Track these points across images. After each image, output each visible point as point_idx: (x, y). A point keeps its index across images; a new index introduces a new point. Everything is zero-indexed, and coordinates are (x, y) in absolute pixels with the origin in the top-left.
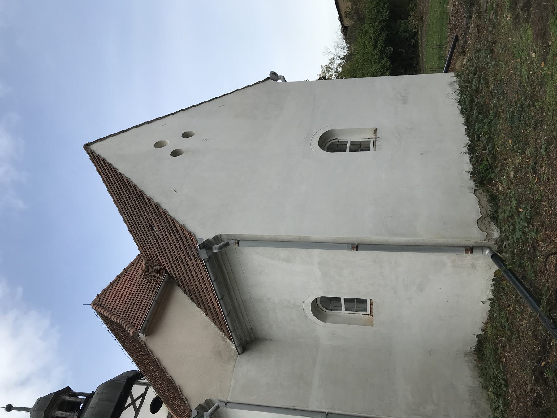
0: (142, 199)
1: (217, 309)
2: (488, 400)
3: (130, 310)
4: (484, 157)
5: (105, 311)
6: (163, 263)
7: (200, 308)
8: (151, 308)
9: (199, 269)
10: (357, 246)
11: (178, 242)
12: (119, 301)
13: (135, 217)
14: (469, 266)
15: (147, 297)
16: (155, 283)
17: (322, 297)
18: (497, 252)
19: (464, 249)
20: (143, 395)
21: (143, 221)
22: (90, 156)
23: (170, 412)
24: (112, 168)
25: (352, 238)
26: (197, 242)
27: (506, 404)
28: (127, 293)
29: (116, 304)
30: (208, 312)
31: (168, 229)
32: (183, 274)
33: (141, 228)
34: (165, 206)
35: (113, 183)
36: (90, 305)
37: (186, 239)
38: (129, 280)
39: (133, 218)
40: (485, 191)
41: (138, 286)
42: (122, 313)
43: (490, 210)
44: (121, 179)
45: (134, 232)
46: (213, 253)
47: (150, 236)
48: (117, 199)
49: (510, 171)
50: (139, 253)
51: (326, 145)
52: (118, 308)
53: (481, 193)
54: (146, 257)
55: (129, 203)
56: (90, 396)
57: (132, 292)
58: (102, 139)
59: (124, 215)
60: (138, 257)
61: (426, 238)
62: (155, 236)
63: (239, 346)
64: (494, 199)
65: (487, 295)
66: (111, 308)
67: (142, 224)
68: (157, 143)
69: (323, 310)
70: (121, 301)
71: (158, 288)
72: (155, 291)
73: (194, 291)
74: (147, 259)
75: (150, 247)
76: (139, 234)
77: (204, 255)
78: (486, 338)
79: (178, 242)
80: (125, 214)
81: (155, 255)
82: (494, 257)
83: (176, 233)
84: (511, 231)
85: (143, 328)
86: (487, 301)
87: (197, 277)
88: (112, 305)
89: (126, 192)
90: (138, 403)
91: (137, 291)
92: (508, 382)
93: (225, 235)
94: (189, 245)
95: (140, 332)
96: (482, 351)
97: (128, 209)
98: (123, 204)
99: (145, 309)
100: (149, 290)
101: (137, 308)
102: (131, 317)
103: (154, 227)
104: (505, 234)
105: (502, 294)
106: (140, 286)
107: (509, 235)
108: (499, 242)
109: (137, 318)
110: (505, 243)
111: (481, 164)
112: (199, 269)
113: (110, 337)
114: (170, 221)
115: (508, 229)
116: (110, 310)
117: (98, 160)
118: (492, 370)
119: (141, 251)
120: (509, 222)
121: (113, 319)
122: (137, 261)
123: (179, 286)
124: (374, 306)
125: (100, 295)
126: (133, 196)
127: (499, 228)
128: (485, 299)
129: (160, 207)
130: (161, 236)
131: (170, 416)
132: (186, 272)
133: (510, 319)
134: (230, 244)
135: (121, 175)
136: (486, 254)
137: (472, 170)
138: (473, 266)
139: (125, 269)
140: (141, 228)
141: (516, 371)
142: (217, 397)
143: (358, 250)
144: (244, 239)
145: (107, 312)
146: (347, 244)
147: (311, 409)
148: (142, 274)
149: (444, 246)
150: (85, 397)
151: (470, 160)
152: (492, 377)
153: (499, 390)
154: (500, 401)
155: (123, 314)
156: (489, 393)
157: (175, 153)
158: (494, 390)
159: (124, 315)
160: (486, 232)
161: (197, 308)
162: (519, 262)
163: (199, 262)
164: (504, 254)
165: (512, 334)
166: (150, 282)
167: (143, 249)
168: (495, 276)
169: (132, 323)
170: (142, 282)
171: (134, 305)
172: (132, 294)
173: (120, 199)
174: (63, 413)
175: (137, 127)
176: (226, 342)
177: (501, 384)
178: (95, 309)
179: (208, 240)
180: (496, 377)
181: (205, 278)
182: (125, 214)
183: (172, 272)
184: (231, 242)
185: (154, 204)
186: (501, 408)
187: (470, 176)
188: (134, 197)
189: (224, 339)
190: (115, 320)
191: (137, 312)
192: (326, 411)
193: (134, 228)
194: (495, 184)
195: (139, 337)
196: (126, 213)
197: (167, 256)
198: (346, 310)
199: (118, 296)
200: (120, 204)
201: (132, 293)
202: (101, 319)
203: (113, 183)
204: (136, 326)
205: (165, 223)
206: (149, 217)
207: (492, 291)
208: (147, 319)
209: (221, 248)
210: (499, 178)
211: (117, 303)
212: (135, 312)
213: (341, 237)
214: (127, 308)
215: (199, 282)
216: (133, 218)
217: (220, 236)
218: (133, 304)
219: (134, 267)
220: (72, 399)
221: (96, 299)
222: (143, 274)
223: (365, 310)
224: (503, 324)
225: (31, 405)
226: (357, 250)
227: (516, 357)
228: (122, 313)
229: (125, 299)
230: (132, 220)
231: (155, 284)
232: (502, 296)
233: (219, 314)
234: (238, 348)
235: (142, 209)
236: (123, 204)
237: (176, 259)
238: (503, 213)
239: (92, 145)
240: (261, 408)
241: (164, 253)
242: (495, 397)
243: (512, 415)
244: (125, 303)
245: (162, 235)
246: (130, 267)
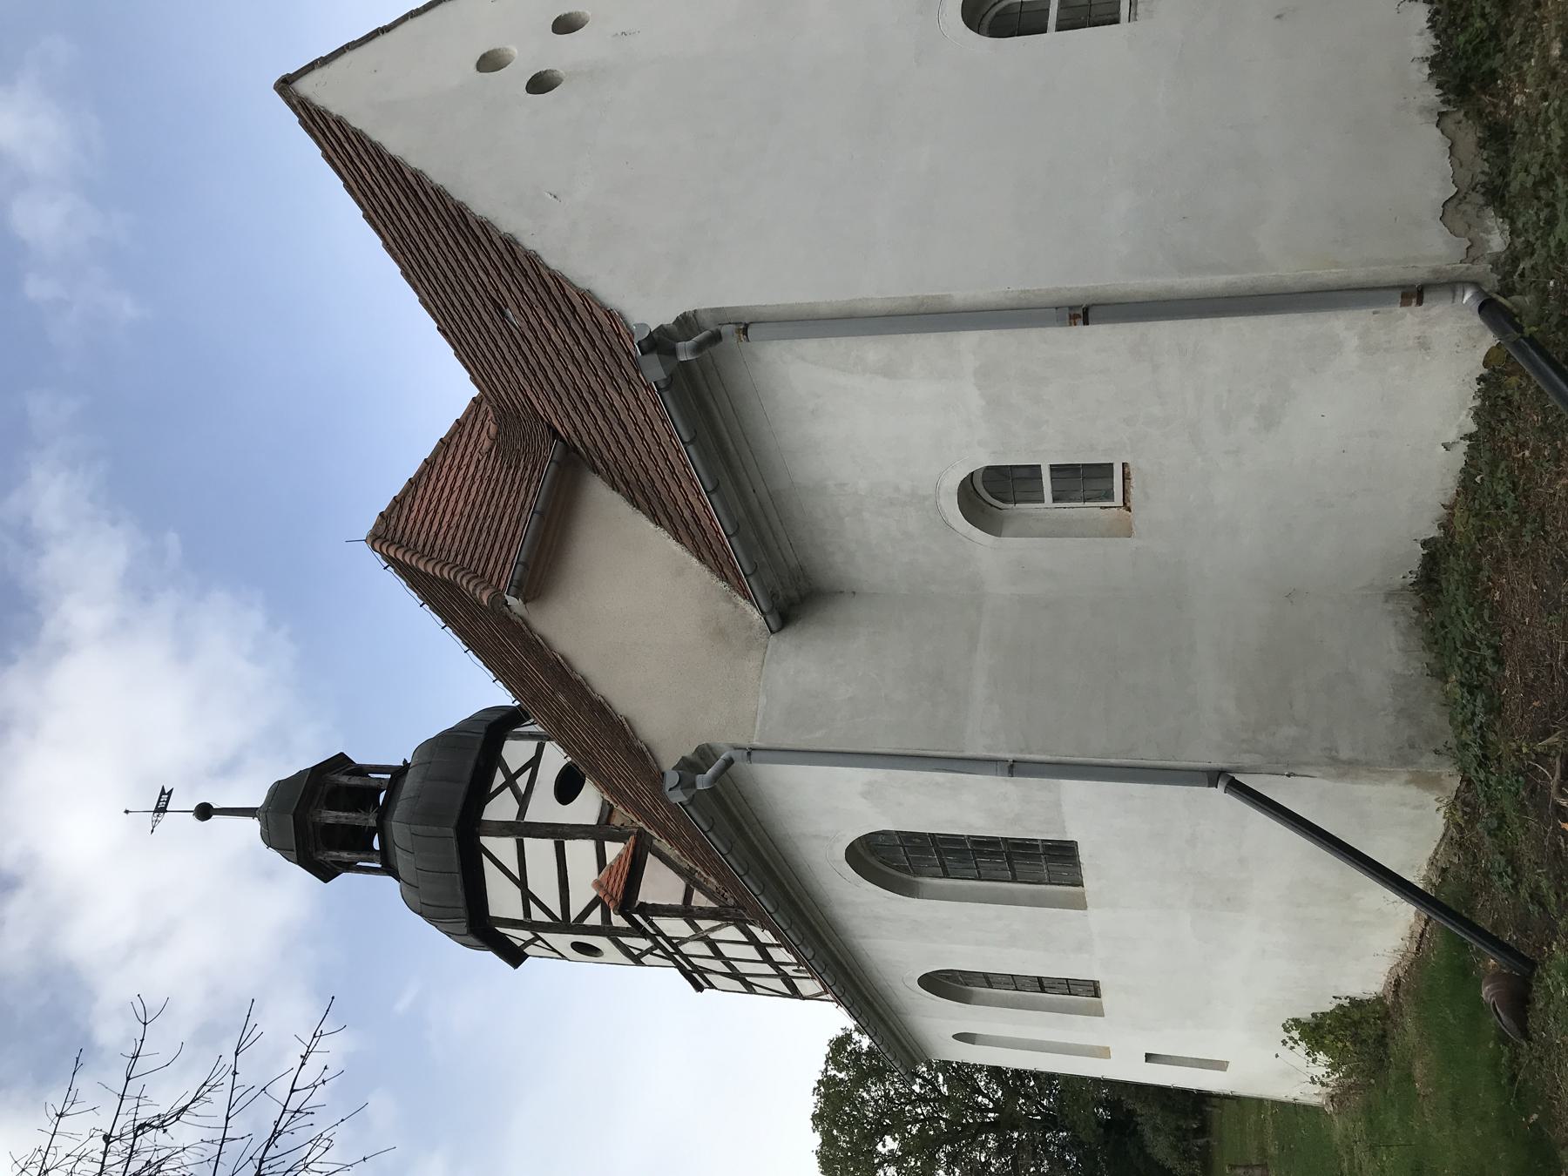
0: (463, 228)
1: (705, 522)
2: (1445, 705)
3: (472, 545)
4: (1472, 7)
5: (405, 552)
6: (545, 410)
7: (659, 523)
8: (549, 471)
9: (645, 414)
10: (1086, 311)
11: (579, 344)
12: (440, 524)
13: (452, 287)
14: (1410, 343)
15: (514, 506)
16: (529, 467)
17: (988, 468)
18: (1498, 293)
19: (1398, 294)
20: (534, 763)
21: (473, 295)
22: (299, 115)
23: (606, 797)
24: (368, 144)
25: (1069, 290)
26: (631, 335)
27: (1495, 709)
28: (457, 502)
29: (432, 533)
30: (682, 532)
31: (546, 309)
32: (603, 437)
33: (471, 318)
34: (530, 241)
35: (377, 190)
36: (365, 541)
37: (602, 332)
38: (459, 468)
39: (445, 291)
40: (1471, 114)
41: (485, 482)
42: (453, 554)
43: (1483, 172)
44: (397, 175)
45: (452, 332)
46: (678, 365)
47: (498, 338)
48: (394, 240)
49: (1551, 40)
50: (475, 392)
51: (984, 16)
52: (439, 541)
53: (1460, 122)
54: (497, 400)
55: (428, 248)
56: (399, 773)
57: (472, 497)
58: (324, 61)
59: (419, 286)
60: (473, 404)
61: (1285, 271)
62: (511, 334)
63: (771, 612)
64: (1497, 137)
65: (1460, 426)
66: (421, 543)
67: (472, 304)
68: (483, 57)
69: (992, 505)
70: (445, 524)
71: (539, 481)
72: (532, 489)
73: (638, 480)
74: (498, 405)
75: (501, 369)
76: (467, 335)
77: (654, 370)
78: (1449, 545)
79: (579, 344)
80: (420, 281)
81: (519, 392)
82: (1488, 309)
83: (570, 317)
84: (1541, 224)
85: (514, 583)
86: (1458, 442)
87: (643, 439)
88: (423, 536)
89: (418, 214)
90: (522, 782)
91: (485, 493)
92: (1503, 653)
93: (705, 310)
94: (611, 349)
95: (507, 594)
96: (1436, 582)
97: (427, 263)
98: (411, 252)
99: (514, 535)
100: (515, 488)
101: (491, 538)
102: (479, 560)
103: (508, 310)
104: (1523, 238)
105: (1503, 416)
106: (489, 481)
107: (1537, 239)
108: (1504, 264)
109: (496, 562)
110: (1521, 266)
111: (1464, 29)
112: (645, 414)
113: (429, 621)
114: (551, 283)
115: (1535, 218)
116: (420, 549)
117: (322, 126)
118: (1460, 626)
119: (478, 386)
120: (1538, 198)
121: (430, 570)
122: (472, 416)
123: (596, 470)
124: (1134, 482)
125: (385, 514)
126: (438, 221)
127: (1507, 220)
128: (1452, 435)
129: (518, 244)
130: (529, 334)
131: (608, 807)
132: (611, 429)
133: (1521, 482)
134: (723, 335)
135: (395, 161)
136: (1464, 302)
137: (1434, 53)
138: (1424, 345)
139: (441, 440)
140: (471, 318)
141: (1527, 619)
142: (725, 738)
143: (1090, 322)
144: (762, 319)
145: (413, 555)
146: (1057, 308)
147: (969, 753)
148: (491, 450)
149: (1341, 290)
150: (389, 776)
151: (1429, 20)
152: (1459, 645)
153: (1478, 676)
154: (1479, 703)
155: (456, 556)
156: (1448, 687)
157: (540, 84)
158: (1462, 675)
159: (460, 557)
160: (1467, 239)
161: (652, 526)
162: (1560, 315)
163: (642, 394)
164: (1515, 298)
165: (1523, 522)
166: (517, 467)
167: (483, 380)
168: (1485, 364)
169: (483, 574)
170: (493, 470)
171: (480, 530)
172: (473, 504)
173: (402, 238)
174: (341, 814)
175: (417, 15)
176: (736, 605)
177: (1484, 658)
178: (378, 550)
179: (661, 329)
180: (1470, 643)
181: (665, 438)
182: (420, 281)
183: (572, 433)
184: (725, 330)
185: (500, 237)
186: (1481, 718)
187: (1427, 71)
188: (440, 225)
189: (729, 599)
190: (438, 574)
191: (493, 546)
192: (1010, 756)
193: (453, 319)
194: (1504, 88)
195: (508, 606)
196: (422, 277)
197: (554, 390)
198: (1055, 500)
199: (436, 512)
200: (403, 254)
201: (470, 500)
202: (400, 575)
203: (377, 190)
204: (494, 582)
205: (536, 292)
206: (490, 281)
207: (1476, 413)
208: (521, 559)
209: (699, 348)
210: (1516, 70)
211: (434, 528)
212: (488, 546)
213: (1039, 290)
214: (465, 540)
215: (650, 452)
216: (445, 291)
217: (694, 316)
218: (477, 528)
219: (466, 432)
220: (356, 781)
221: (376, 526)
222: (494, 450)
223: (1109, 495)
224: (1501, 498)
225: (258, 801)
226: (1086, 323)
227: (1531, 580)
228: (453, 554)
229: (456, 518)
230: (443, 296)
231: (529, 469)
232: (1502, 422)
233: (710, 534)
234: (768, 618)
235: (467, 260)
236: (411, 252)
237: (579, 395)
238: (1522, 175)
239: (299, 80)
240: (841, 757)
241: (544, 383)
242: (1466, 694)
243: (1510, 733)
244: (458, 527)
245: (532, 330)
246: (455, 433)
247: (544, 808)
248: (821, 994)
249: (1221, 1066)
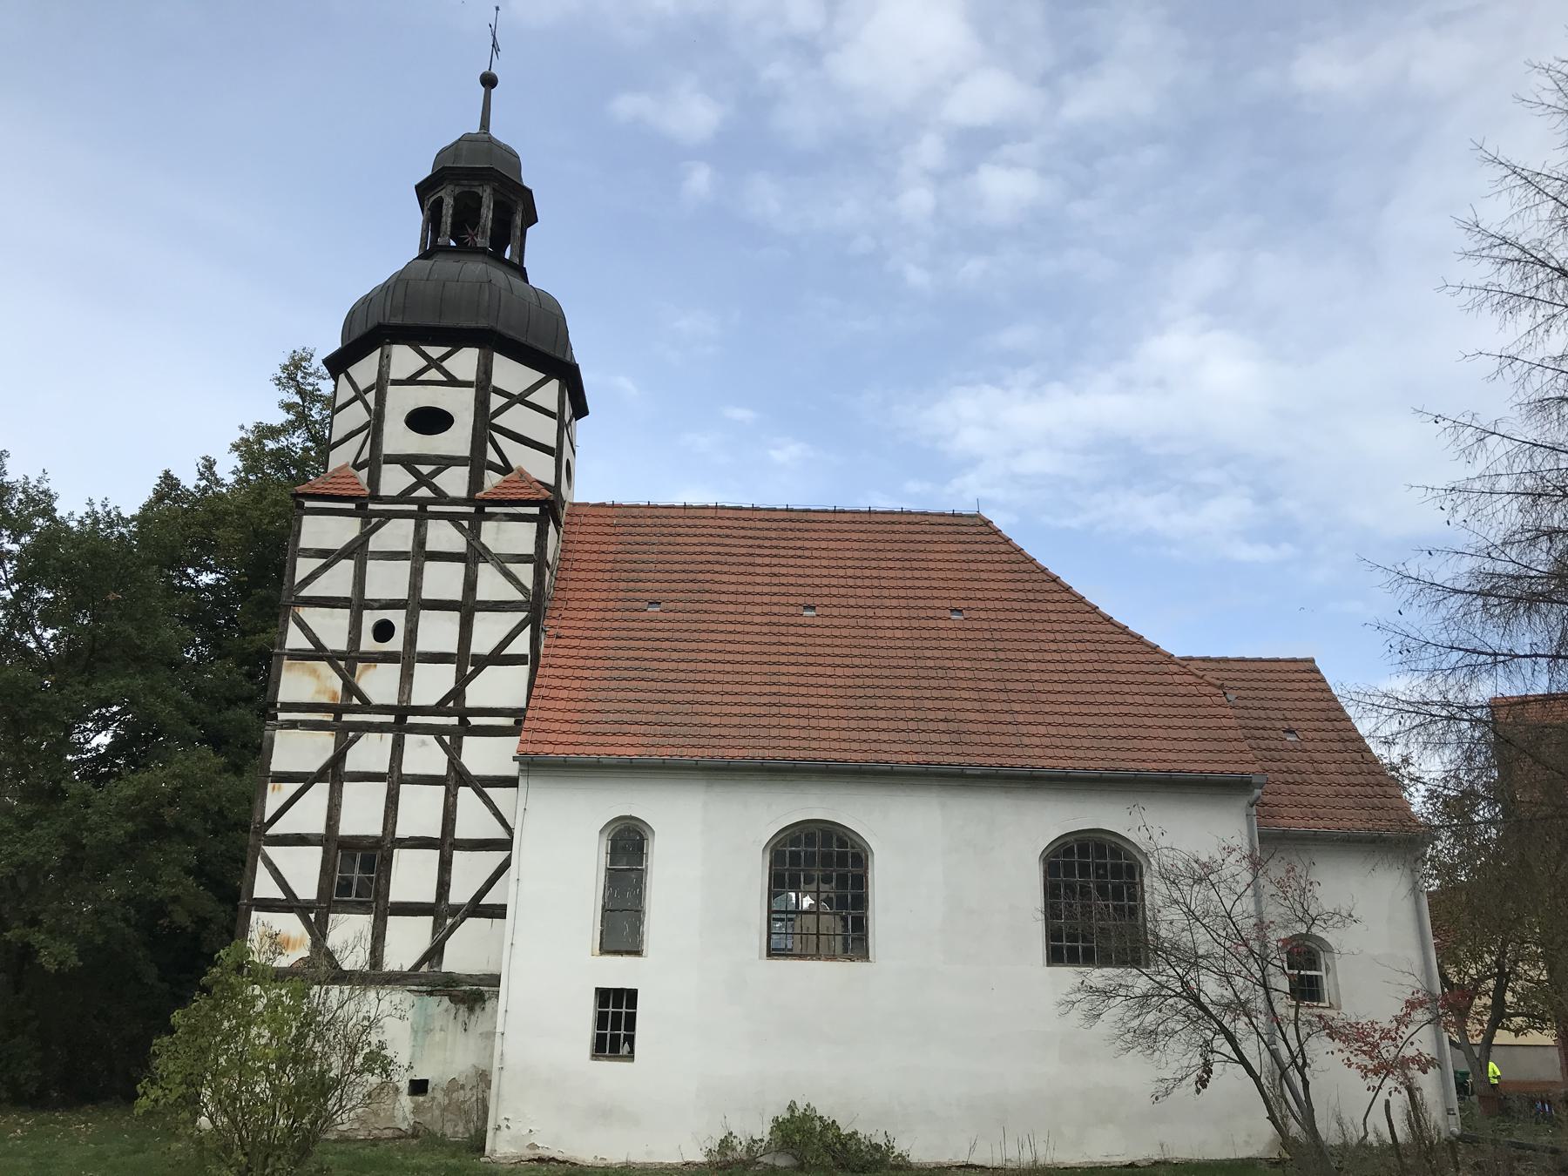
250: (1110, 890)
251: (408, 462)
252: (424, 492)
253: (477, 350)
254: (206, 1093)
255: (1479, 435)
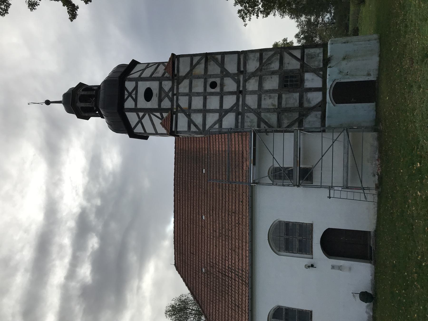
20: (136, 88)
247: (142, 103)
248: (142, 74)
249: (333, 267)
250: (297, 83)
251: (160, 101)
252: (170, 94)
253: (126, 82)
254: (408, 211)
255: (232, 267)
